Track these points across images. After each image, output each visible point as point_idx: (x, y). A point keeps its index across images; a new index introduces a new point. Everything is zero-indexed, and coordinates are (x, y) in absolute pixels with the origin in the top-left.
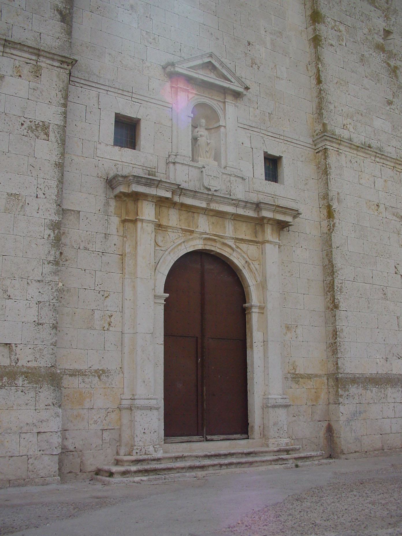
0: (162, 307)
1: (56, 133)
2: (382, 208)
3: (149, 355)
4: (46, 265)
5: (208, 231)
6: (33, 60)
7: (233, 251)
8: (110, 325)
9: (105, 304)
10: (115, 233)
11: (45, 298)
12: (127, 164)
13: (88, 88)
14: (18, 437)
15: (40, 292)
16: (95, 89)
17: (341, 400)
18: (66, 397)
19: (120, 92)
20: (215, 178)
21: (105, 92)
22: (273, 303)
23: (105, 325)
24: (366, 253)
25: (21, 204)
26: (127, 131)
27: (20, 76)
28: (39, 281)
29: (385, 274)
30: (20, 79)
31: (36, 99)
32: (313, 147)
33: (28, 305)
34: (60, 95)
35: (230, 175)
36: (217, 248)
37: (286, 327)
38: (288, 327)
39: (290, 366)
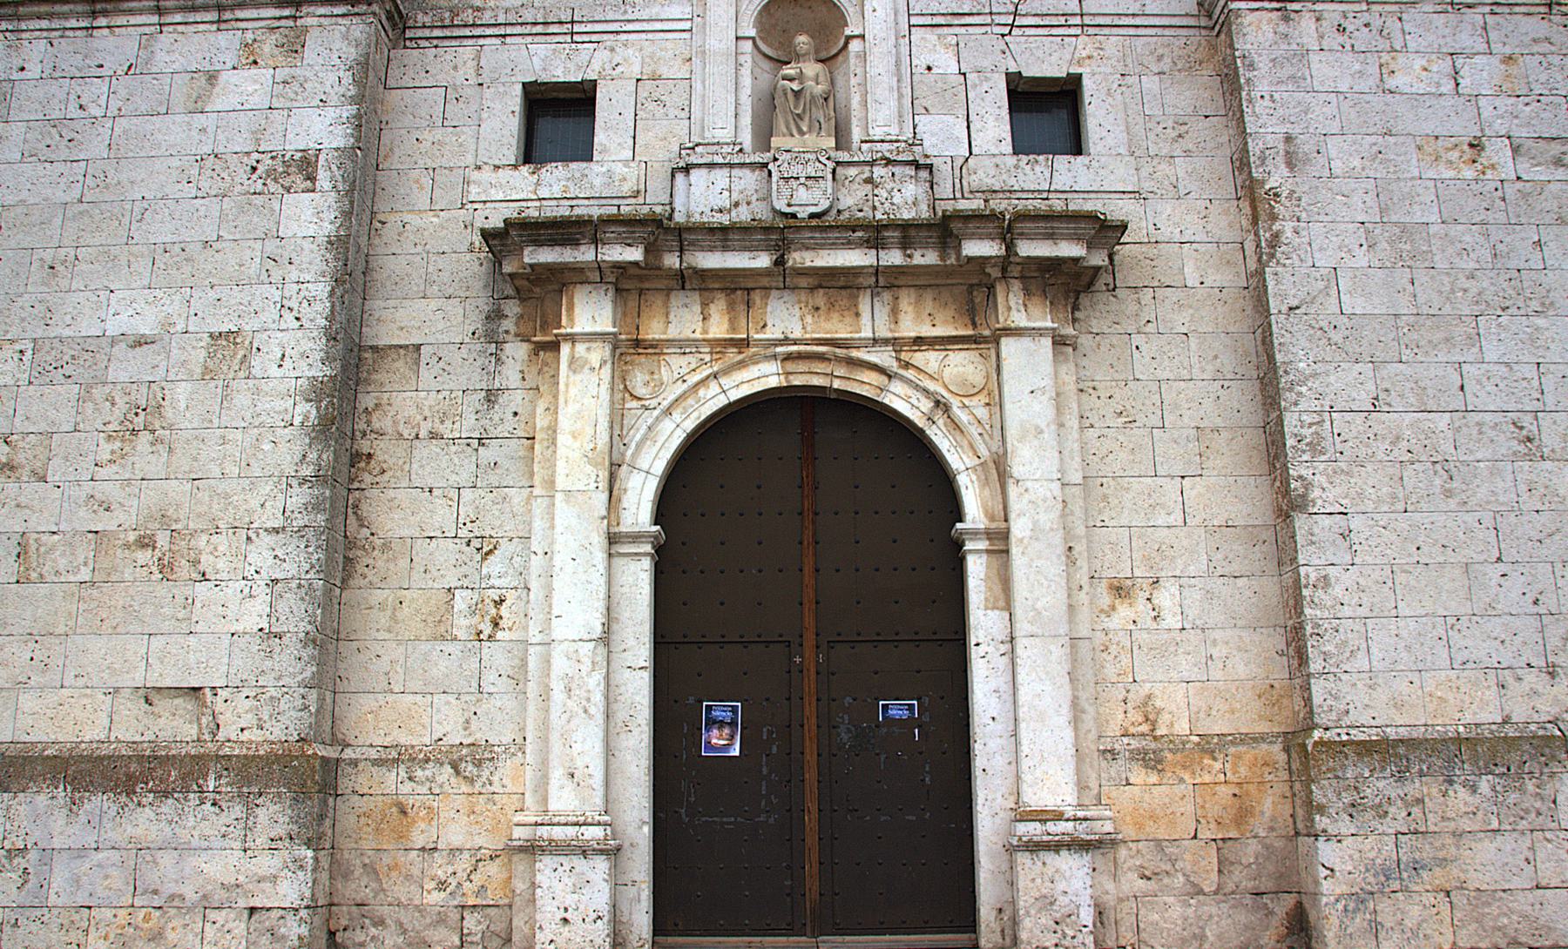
0: (647, 563)
1: (334, 168)
2: (1498, 152)
3: (588, 700)
4: (296, 489)
5: (797, 334)
6: (286, 18)
7: (890, 377)
8: (496, 624)
9: (484, 571)
10: (518, 384)
11: (290, 569)
12: (554, 203)
13: (454, 43)
14: (199, 919)
15: (276, 557)
16: (470, 42)
17: (1321, 822)
18: (363, 820)
19: (539, 29)
20: (809, 183)
21: (497, 41)
22: (1033, 516)
23: (481, 627)
24: (1425, 310)
25: (241, 353)
26: (558, 117)
27: (255, 62)
28: (276, 531)
29: (1530, 372)
30: (254, 71)
31: (288, 105)
32: (1204, 22)
33: (247, 591)
34: (347, 78)
35: (872, 163)
36: (840, 381)
37: (1111, 587)
38: (1119, 589)
39: (1131, 713)
